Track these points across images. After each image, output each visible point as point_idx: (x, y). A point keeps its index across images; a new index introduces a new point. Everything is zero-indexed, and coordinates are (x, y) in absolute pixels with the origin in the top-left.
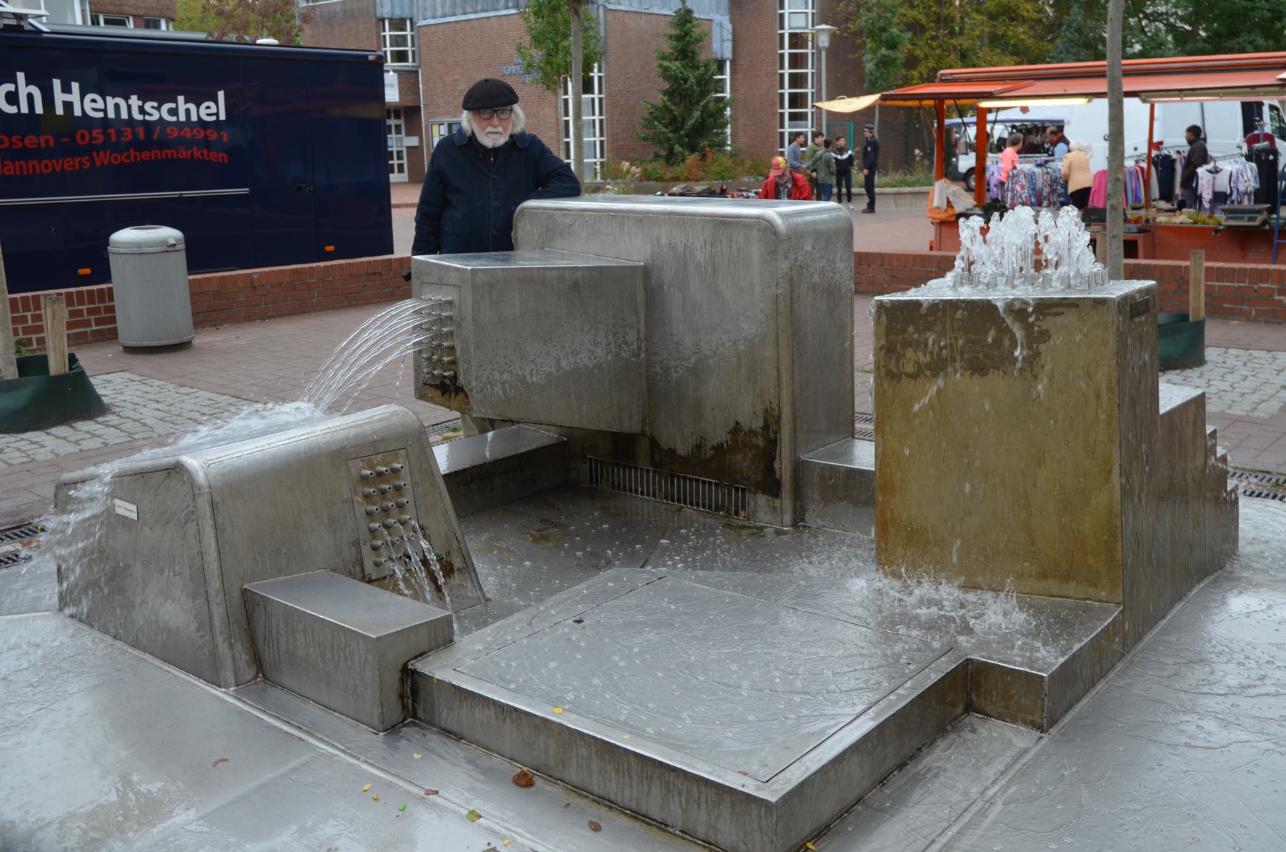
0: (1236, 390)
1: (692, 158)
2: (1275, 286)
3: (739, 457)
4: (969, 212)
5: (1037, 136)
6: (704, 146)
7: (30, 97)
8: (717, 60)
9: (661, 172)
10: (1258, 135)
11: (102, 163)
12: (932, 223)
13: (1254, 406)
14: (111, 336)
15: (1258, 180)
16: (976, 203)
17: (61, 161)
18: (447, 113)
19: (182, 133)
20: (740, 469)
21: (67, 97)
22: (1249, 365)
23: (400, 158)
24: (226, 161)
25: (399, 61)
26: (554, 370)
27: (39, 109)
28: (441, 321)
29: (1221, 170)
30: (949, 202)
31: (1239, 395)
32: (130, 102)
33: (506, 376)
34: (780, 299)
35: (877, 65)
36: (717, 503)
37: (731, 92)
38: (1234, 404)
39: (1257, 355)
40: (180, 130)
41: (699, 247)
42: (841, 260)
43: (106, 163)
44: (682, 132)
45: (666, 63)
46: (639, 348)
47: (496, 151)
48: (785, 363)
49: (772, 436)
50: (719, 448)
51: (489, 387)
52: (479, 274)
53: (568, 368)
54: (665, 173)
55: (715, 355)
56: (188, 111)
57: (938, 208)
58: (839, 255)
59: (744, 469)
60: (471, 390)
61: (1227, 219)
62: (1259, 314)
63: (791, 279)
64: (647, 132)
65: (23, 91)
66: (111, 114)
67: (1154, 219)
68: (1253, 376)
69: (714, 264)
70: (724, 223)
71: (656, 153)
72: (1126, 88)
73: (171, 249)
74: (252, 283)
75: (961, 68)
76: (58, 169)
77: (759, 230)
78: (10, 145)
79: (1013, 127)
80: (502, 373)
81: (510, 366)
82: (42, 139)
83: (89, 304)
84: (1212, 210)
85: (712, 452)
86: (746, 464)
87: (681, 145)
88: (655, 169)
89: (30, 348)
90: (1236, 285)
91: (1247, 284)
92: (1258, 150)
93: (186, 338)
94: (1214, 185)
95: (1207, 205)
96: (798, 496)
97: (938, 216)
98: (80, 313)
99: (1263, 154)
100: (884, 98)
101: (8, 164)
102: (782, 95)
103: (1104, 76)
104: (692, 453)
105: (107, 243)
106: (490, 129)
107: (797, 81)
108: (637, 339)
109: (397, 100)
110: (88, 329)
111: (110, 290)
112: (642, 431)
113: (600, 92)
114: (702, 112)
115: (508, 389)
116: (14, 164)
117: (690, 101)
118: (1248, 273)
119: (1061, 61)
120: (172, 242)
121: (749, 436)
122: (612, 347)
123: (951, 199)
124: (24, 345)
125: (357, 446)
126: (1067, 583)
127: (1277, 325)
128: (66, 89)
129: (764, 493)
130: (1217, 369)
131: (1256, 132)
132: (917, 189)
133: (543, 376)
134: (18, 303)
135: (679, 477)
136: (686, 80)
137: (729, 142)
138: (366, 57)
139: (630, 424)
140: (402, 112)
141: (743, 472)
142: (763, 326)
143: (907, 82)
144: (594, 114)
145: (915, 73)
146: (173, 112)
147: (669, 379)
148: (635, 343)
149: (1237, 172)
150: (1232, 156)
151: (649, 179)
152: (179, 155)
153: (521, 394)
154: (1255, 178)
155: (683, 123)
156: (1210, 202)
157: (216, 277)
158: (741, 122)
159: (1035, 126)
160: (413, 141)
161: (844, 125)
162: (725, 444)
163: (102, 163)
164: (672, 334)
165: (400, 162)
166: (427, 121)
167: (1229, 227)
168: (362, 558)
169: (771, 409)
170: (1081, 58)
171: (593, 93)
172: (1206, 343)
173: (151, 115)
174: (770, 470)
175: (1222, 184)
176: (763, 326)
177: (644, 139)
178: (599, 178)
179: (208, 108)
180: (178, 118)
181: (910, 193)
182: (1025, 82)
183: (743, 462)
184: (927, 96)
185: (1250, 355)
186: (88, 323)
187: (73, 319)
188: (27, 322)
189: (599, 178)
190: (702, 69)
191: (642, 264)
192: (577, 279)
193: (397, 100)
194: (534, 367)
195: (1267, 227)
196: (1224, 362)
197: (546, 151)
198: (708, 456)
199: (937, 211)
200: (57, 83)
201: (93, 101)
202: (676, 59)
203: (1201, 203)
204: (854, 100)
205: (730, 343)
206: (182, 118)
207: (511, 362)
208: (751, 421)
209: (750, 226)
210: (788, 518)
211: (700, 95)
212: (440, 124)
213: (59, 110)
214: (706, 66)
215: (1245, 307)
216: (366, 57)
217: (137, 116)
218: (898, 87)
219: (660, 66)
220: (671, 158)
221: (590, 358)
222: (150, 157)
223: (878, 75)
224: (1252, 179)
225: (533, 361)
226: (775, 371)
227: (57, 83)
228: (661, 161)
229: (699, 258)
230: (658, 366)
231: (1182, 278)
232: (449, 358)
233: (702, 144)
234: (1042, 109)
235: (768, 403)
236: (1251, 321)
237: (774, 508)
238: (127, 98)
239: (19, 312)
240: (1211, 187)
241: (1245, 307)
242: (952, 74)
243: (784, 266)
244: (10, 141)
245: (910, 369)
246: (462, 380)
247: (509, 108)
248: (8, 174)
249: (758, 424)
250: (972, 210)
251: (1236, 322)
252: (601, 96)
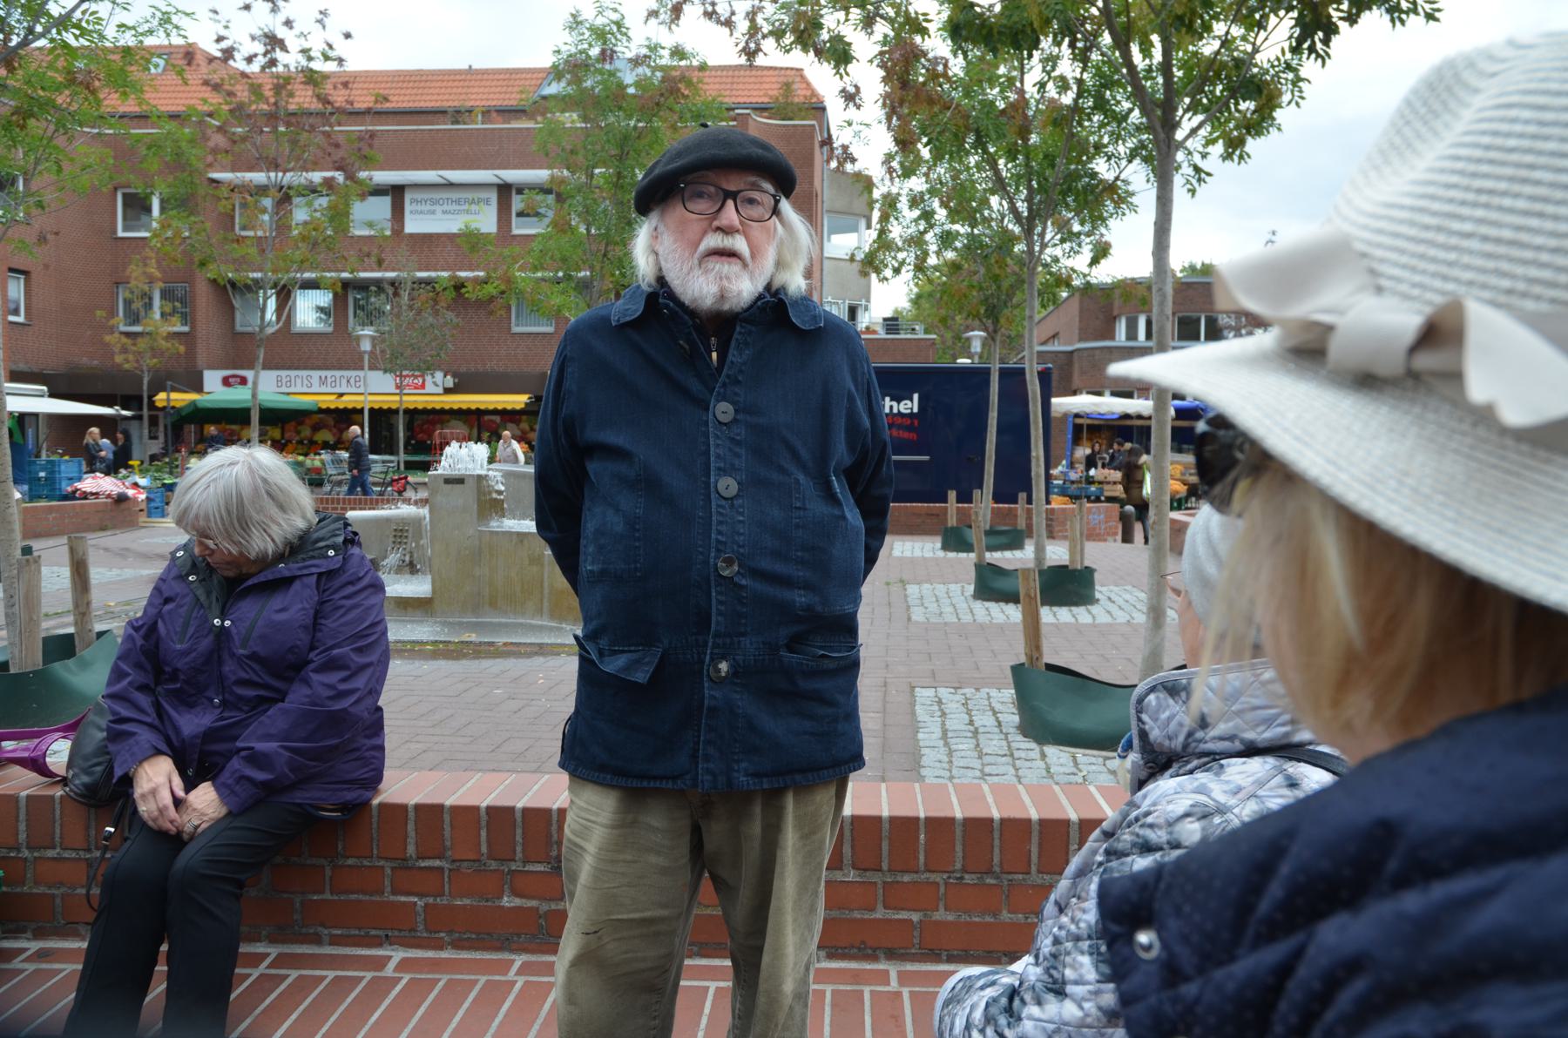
56: (891, 407)
106: (713, 241)
187: (931, 989)
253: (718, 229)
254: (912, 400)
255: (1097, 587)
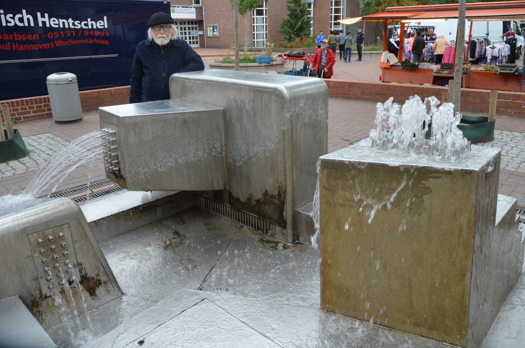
0: (509, 155)
1: (298, 39)
2: (523, 102)
3: (267, 207)
4: (396, 64)
5: (424, 32)
6: (302, 35)
7: (28, 19)
8: (308, 3)
9: (286, 44)
10: (509, 33)
11: (59, 45)
12: (381, 68)
13: (518, 165)
14: (50, 116)
15: (510, 51)
16: (398, 61)
17: (42, 45)
18: (212, 23)
19: (90, 33)
20: (268, 213)
21: (43, 20)
22: (513, 140)
23: (197, 39)
24: (108, 44)
25: (197, 4)
26: (174, 164)
27: (32, 24)
28: (113, 142)
29: (496, 47)
30: (388, 60)
31: (511, 158)
32: (69, 21)
33: (146, 170)
34: (286, 132)
35: (365, 5)
36: (258, 226)
37: (313, 15)
38: (509, 164)
39: (516, 135)
40: (89, 32)
41: (247, 102)
42: (321, 109)
43: (60, 45)
44: (294, 30)
45: (289, 4)
46: (222, 150)
47: (164, 47)
48: (288, 164)
49: (282, 200)
50: (258, 201)
51: (136, 175)
52: (127, 119)
53: (182, 163)
54: (288, 45)
55: (256, 157)
57: (383, 63)
58: (320, 107)
59: (269, 213)
60: (126, 178)
61: (500, 70)
62: (515, 113)
63: (292, 121)
64: (282, 30)
65: (25, 17)
66: (61, 26)
67: (470, 69)
68: (516, 147)
69: (255, 111)
70: (258, 91)
71: (285, 37)
72: (467, 15)
73: (70, 82)
74: (111, 93)
75: (397, 6)
76: (41, 48)
77: (275, 96)
78: (53, 37)
79: (415, 29)
80: (143, 168)
81: (148, 164)
82: (34, 36)
83: (44, 103)
84: (491, 63)
85: (255, 203)
86: (270, 211)
87: (294, 35)
88: (284, 43)
89: (20, 121)
90: (506, 101)
91: (511, 101)
92: (509, 39)
93: (79, 118)
94: (492, 53)
95: (489, 61)
96: (295, 228)
97: (383, 66)
98: (41, 106)
99: (511, 41)
100: (363, 19)
101: (21, 46)
102: (331, 16)
103: (457, 10)
104: (247, 201)
105: (46, 80)
106: (159, 35)
107: (337, 11)
108: (221, 146)
109: (195, 18)
110: (44, 113)
111: (48, 98)
112: (225, 188)
113: (266, 15)
114: (302, 22)
115: (148, 176)
116: (23, 46)
117: (297, 18)
118: (512, 96)
119: (434, 4)
120: (70, 79)
121: (272, 198)
122: (206, 150)
123: (389, 59)
124: (18, 120)
125: (34, 226)
126: (432, 331)
127: (522, 118)
128: (43, 16)
129: (279, 226)
130: (499, 143)
131: (509, 32)
132: (378, 52)
133: (168, 168)
134: (14, 103)
135: (241, 211)
136: (296, 11)
137: (312, 33)
138: (163, 2)
139: (218, 186)
140: (197, 22)
141: (269, 214)
142: (278, 145)
143: (377, 12)
144: (263, 23)
145: (380, 8)
146: (86, 25)
147: (236, 165)
148: (220, 148)
149: (502, 48)
150: (499, 42)
151: (282, 47)
152: (89, 42)
153: (155, 178)
154: (509, 50)
155: (295, 27)
156: (490, 60)
157: (96, 91)
158: (317, 26)
159: (423, 28)
160: (201, 33)
161: (354, 27)
162: (261, 200)
163: (59, 45)
164: (237, 144)
165: (197, 40)
166: (205, 26)
167: (501, 73)
168: (40, 287)
169: (282, 187)
170: (441, 2)
171: (263, 15)
172: (495, 128)
173: (77, 26)
174: (281, 216)
175: (496, 53)
176: (278, 145)
177: (281, 32)
178: (265, 47)
179: (100, 23)
180: (88, 27)
181: (375, 53)
182: (421, 12)
183: (269, 210)
184: (380, 18)
185: (513, 135)
186: (44, 111)
188: (19, 111)
189: (265, 47)
190: (302, 6)
191: (223, 108)
192: (185, 118)
193: (195, 18)
194: (162, 164)
195: (517, 73)
196: (502, 139)
197: (189, 48)
198: (254, 204)
199: (383, 64)
200: (39, 14)
201: (54, 21)
202: (293, 3)
203: (486, 60)
204: (352, 19)
205: (263, 152)
206: (90, 27)
207: (149, 162)
208: (273, 191)
209: (271, 93)
210: (290, 239)
211: (301, 16)
212: (210, 27)
213: (41, 25)
214: (303, 5)
215: (509, 110)
216: (163, 2)
217: (72, 27)
218: (374, 13)
219: (287, 5)
220: (290, 39)
221: (194, 157)
222: (47, 47)
223: (365, 9)
224: (507, 51)
225: (162, 161)
226: (283, 169)
227: (39, 14)
228: (287, 40)
229: (247, 108)
230: (231, 158)
231: (483, 97)
232: (115, 161)
233: (301, 34)
234: (425, 23)
235: (280, 183)
236: (511, 116)
237: (283, 234)
238: (67, 20)
239: (15, 107)
240: (491, 54)
241: (509, 110)
242: (391, 9)
243: (288, 115)
244: (21, 37)
245: (341, 201)
246: (122, 173)
247: (169, 25)
248: (21, 50)
249: (276, 193)
250: (397, 63)
251: (505, 117)
252: (266, 16)
253: (160, 33)
254: (103, 21)
255: (319, 283)
